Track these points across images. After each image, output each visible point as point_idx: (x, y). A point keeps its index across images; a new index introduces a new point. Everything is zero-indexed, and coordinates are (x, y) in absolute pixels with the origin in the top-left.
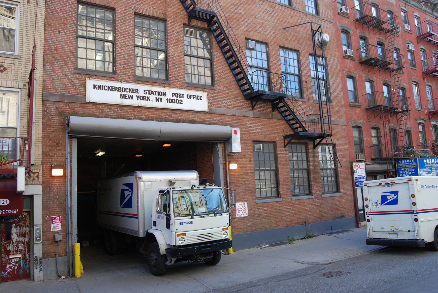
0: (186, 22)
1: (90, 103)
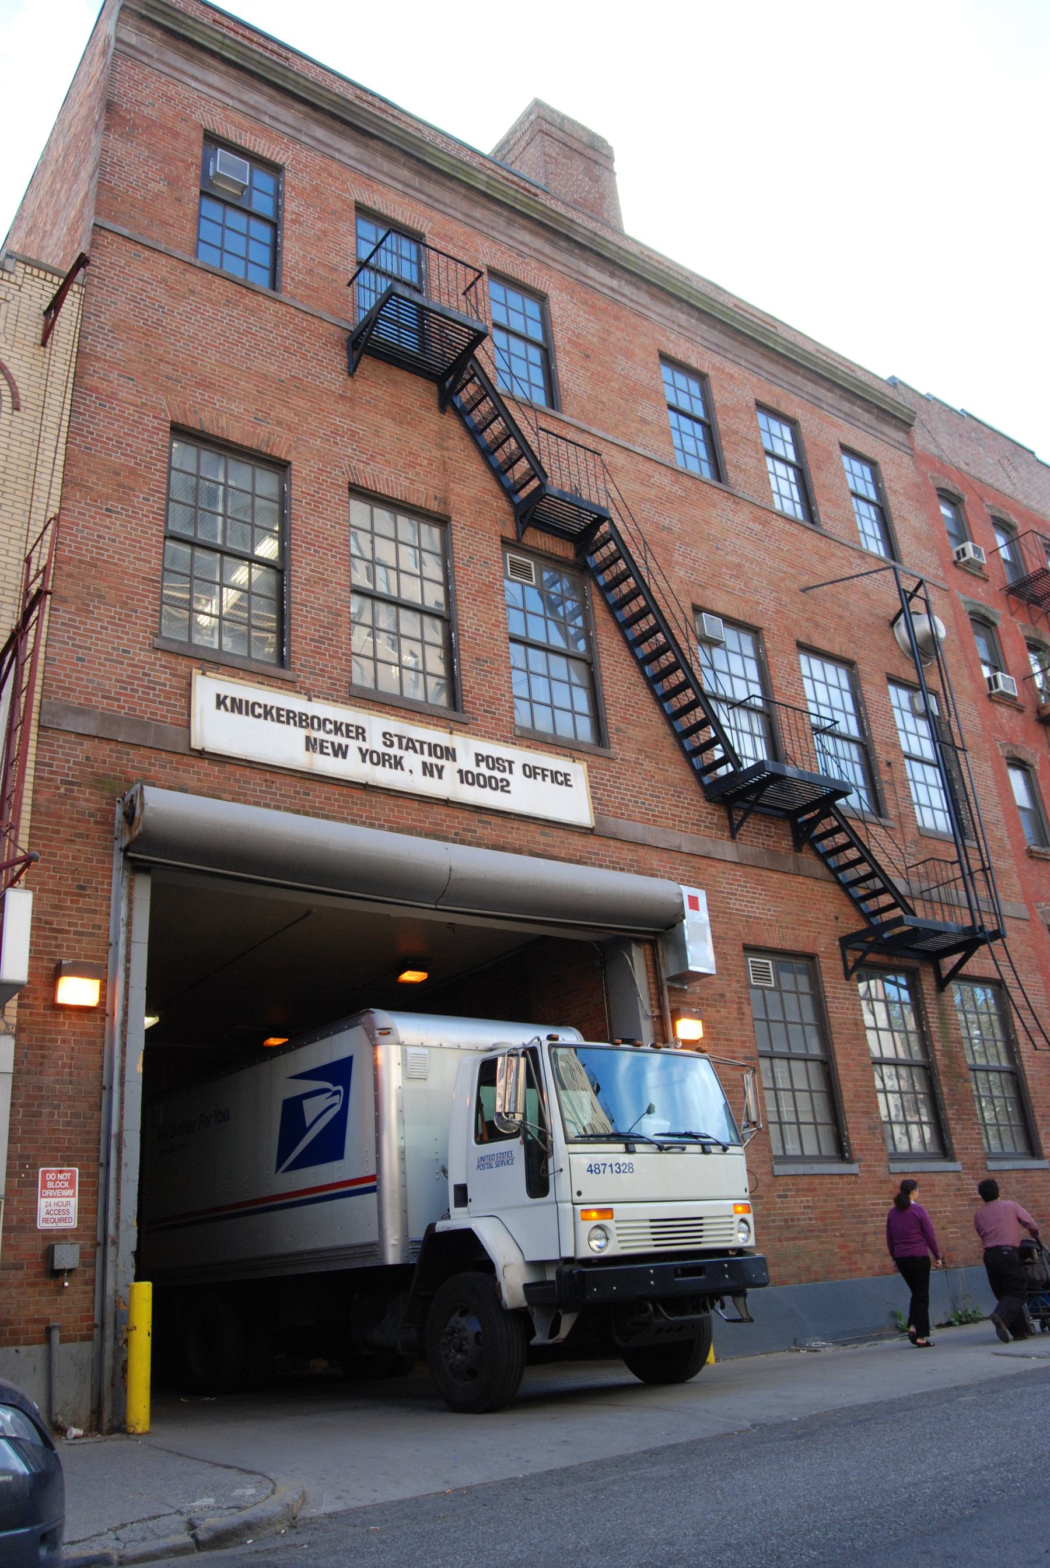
0: (510, 533)
1: (202, 754)
